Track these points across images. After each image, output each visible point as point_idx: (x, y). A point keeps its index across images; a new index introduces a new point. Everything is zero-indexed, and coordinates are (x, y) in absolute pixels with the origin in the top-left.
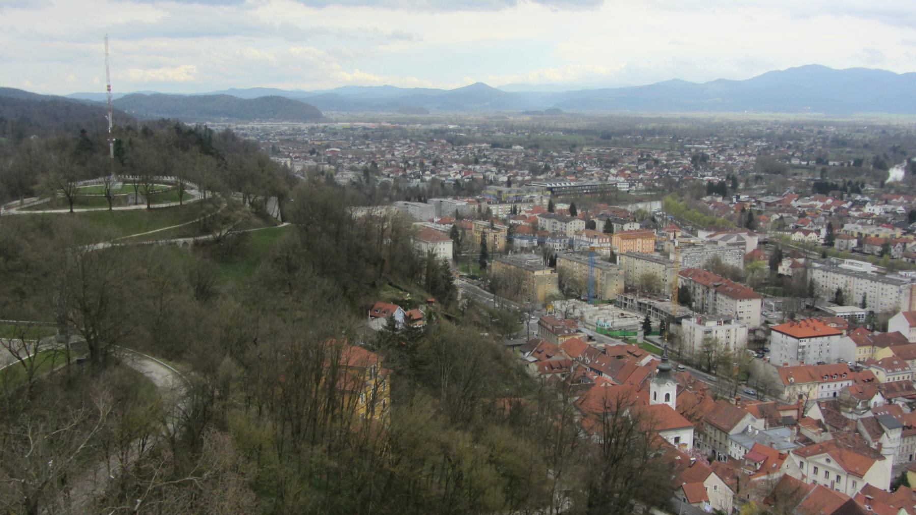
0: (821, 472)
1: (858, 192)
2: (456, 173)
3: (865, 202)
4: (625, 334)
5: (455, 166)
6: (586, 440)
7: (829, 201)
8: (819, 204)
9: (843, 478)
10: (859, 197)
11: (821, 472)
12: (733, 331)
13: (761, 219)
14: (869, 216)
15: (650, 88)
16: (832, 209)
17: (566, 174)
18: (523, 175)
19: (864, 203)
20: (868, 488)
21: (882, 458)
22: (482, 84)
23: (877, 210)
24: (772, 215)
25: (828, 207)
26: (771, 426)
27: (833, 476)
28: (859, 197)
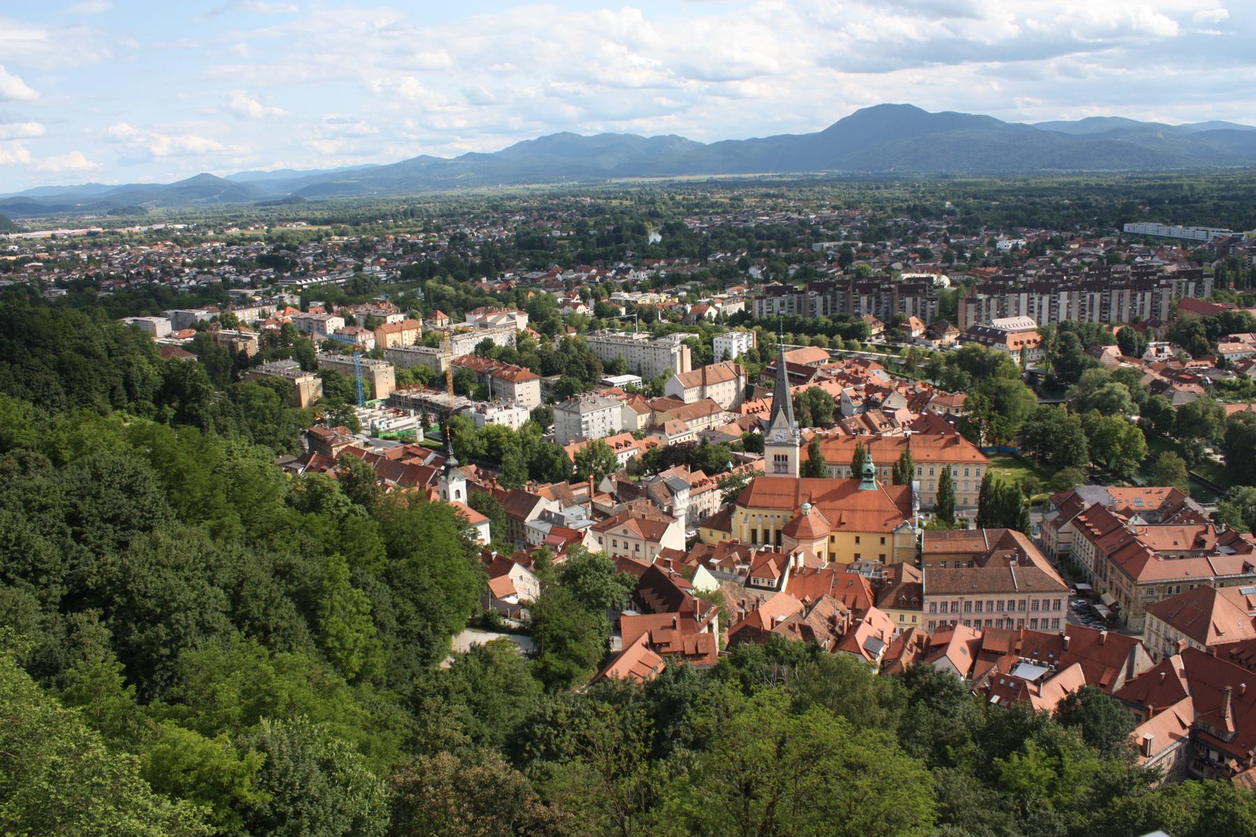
0: (620, 544)
1: (621, 260)
2: (190, 279)
3: (629, 269)
4: (405, 439)
5: (187, 270)
6: (414, 501)
7: (594, 271)
8: (584, 276)
9: (641, 547)
10: (622, 265)
11: (620, 544)
12: (515, 416)
13: (560, 434)
14: (634, 282)
15: (397, 166)
16: (597, 279)
17: (316, 268)
18: (266, 274)
19: (627, 271)
20: (667, 552)
21: (675, 519)
22: (207, 175)
23: (643, 276)
24: (511, 380)
25: (594, 277)
26: (566, 506)
27: (632, 547)
28: (622, 265)
